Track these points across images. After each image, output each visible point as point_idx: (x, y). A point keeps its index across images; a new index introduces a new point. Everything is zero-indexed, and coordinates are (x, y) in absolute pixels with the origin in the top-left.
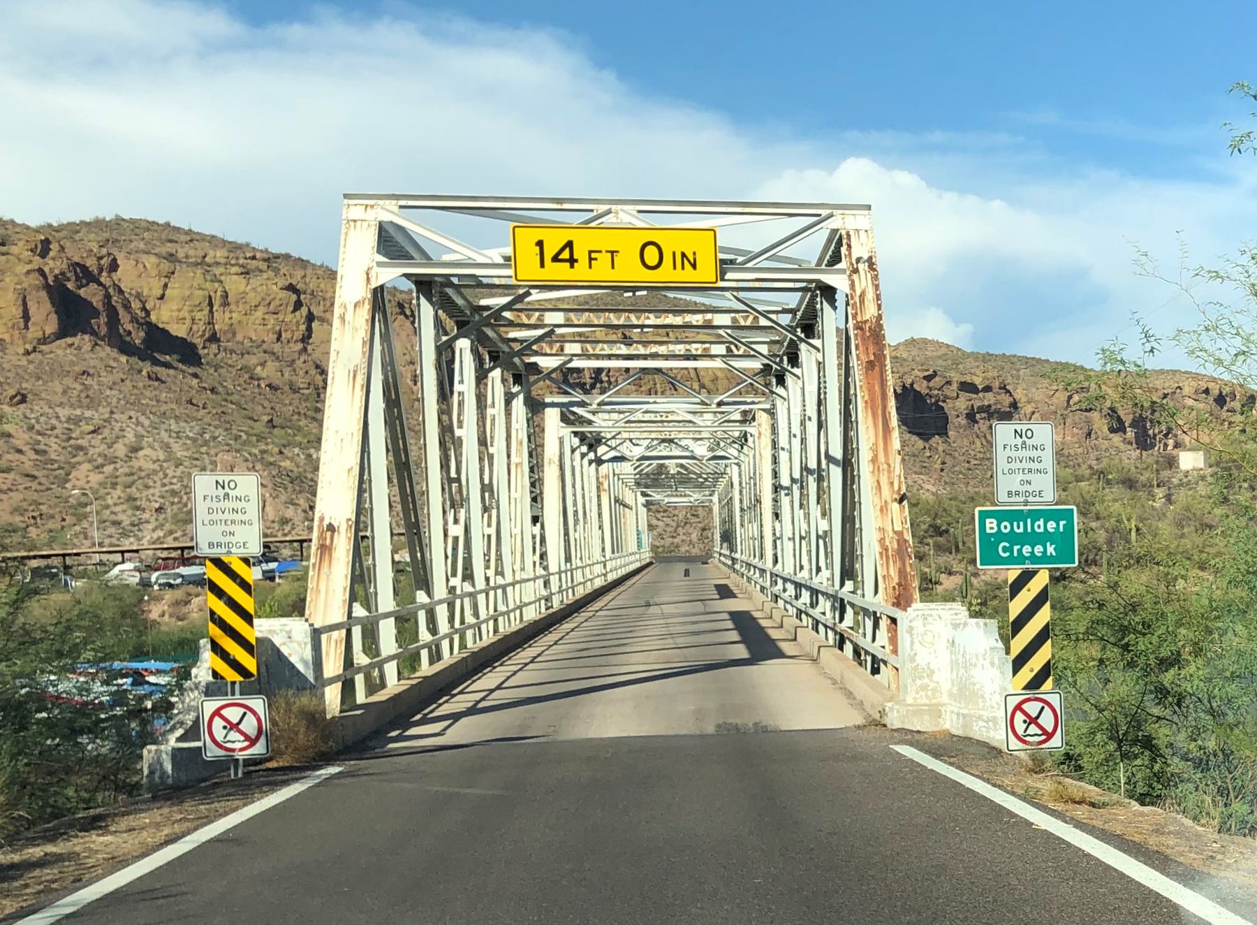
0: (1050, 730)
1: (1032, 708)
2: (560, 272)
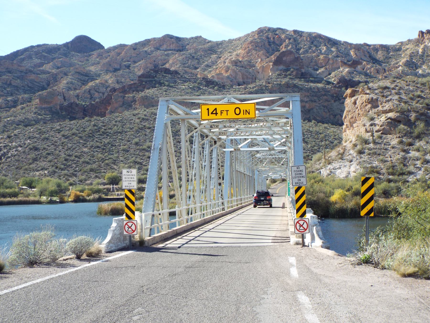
1: (301, 222)
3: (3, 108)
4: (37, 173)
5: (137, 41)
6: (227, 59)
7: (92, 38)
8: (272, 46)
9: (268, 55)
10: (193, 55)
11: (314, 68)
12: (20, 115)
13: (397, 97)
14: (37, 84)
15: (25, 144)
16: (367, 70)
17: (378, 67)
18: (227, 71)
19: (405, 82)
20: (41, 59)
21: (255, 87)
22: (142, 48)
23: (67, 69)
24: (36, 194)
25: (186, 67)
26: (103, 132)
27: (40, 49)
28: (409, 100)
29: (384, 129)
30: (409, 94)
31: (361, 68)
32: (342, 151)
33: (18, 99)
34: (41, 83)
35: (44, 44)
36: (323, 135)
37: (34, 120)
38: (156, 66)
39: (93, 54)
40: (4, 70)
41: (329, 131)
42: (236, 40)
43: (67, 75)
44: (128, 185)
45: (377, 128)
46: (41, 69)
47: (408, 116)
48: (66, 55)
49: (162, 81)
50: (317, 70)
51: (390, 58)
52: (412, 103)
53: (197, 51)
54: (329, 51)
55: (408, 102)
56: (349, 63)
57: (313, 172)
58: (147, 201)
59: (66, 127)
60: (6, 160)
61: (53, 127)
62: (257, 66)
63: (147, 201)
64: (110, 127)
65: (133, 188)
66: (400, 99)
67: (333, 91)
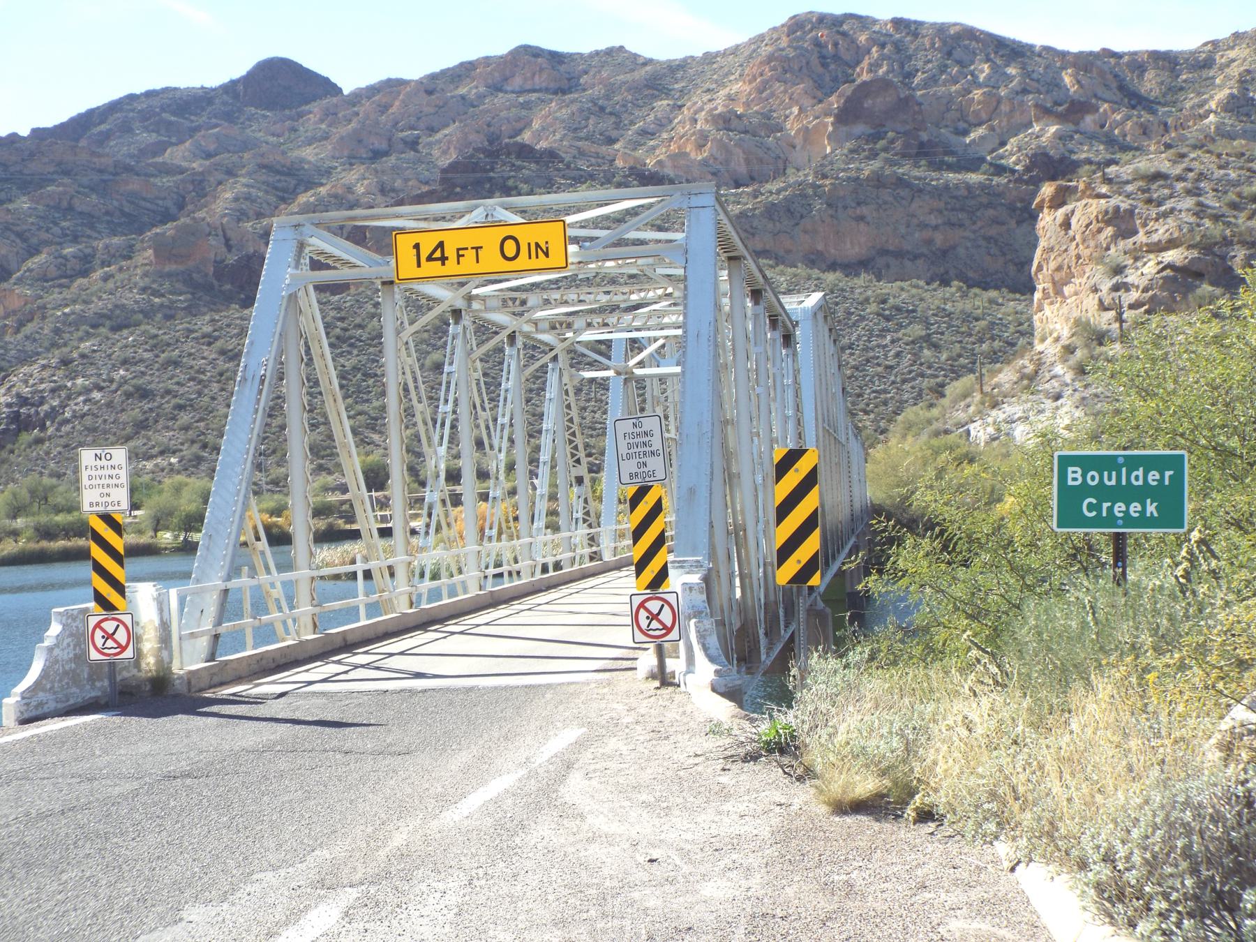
0: (124, 643)
1: (654, 606)
2: (434, 268)
3: (52, 280)
4: (149, 465)
5: (437, 69)
6: (701, 109)
7: (305, 65)
8: (832, 67)
9: (819, 94)
10: (600, 102)
11: (956, 129)
12: (100, 298)
13: (1189, 202)
14: (148, 205)
15: (112, 381)
16: (1112, 129)
17: (1146, 117)
18: (700, 147)
19: (1214, 158)
20: (158, 132)
21: (785, 189)
22: (452, 87)
23: (235, 158)
24: (143, 526)
25: (580, 139)
26: (338, 338)
27: (155, 102)
28: (1225, 210)
29: (1152, 298)
30: (1226, 193)
31: (1094, 121)
32: (1030, 368)
33: (95, 249)
34: (160, 202)
35: (167, 88)
36: (983, 323)
37: (142, 311)
38: (493, 139)
39: (310, 112)
40: (52, 169)
41: (1003, 309)
42: (724, 54)
43: (236, 176)
44: (100, 500)
45: (1134, 295)
46: (160, 160)
47: (1223, 258)
48: (229, 117)
49: (510, 183)
50: (966, 133)
51: (1181, 89)
52: (1235, 217)
53: (611, 90)
54: (999, 76)
55: (1223, 216)
56: (1060, 109)
57: (947, 432)
58: (208, 549)
59: (228, 326)
60: (58, 430)
61: (191, 327)
62: (788, 127)
63: (208, 549)
64: (358, 320)
65: (116, 508)
66: (1198, 208)
67: (1014, 193)
